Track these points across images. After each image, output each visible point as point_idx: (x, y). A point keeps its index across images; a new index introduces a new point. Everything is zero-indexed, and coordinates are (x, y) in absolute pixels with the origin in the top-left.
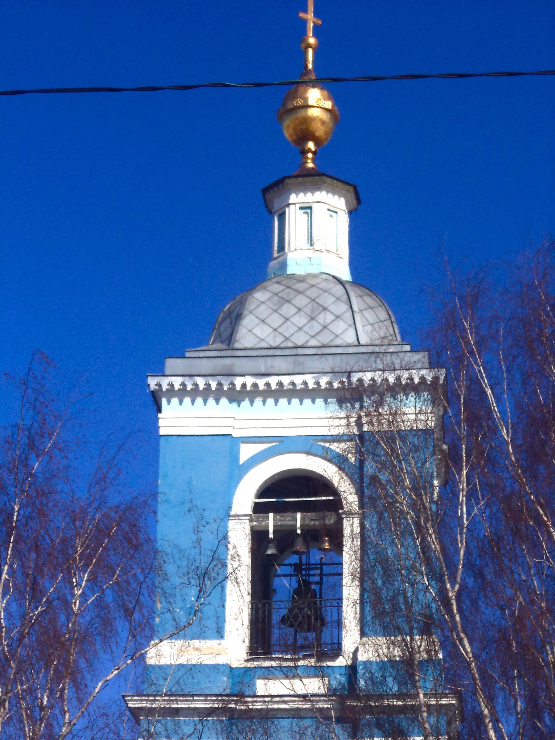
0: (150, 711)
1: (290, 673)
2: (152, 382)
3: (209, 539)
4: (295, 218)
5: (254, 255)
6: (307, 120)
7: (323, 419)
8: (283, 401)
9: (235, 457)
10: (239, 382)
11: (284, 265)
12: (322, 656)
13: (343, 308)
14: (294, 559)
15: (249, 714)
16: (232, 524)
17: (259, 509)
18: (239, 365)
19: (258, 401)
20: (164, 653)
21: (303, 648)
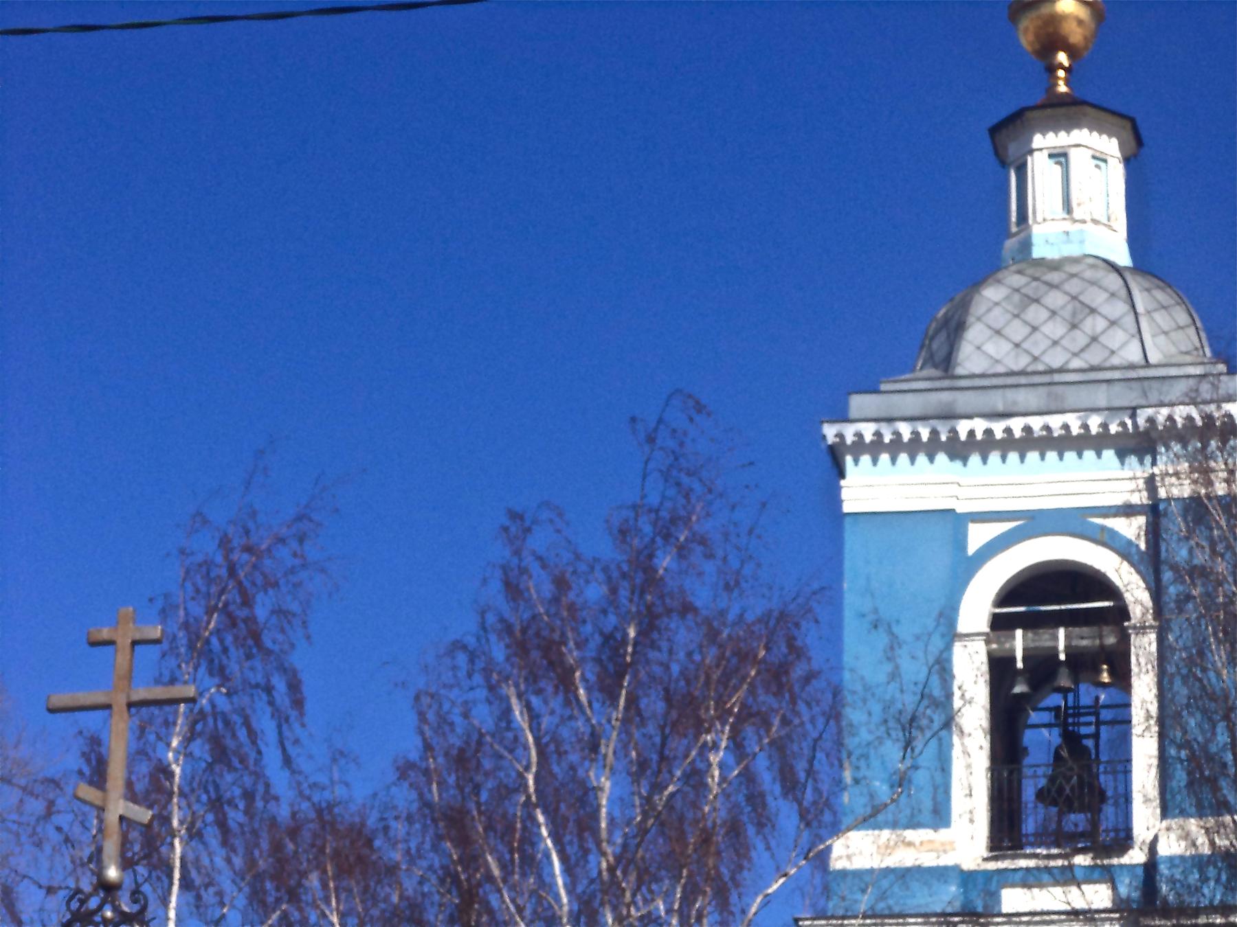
1: (1068, 877)
4: (1042, 171)
5: (987, 236)
7: (1109, 481)
8: (1033, 456)
9: (960, 541)
10: (963, 427)
11: (1027, 245)
13: (1119, 309)
14: (1055, 700)
17: (1000, 624)
18: (963, 401)
20: (856, 850)
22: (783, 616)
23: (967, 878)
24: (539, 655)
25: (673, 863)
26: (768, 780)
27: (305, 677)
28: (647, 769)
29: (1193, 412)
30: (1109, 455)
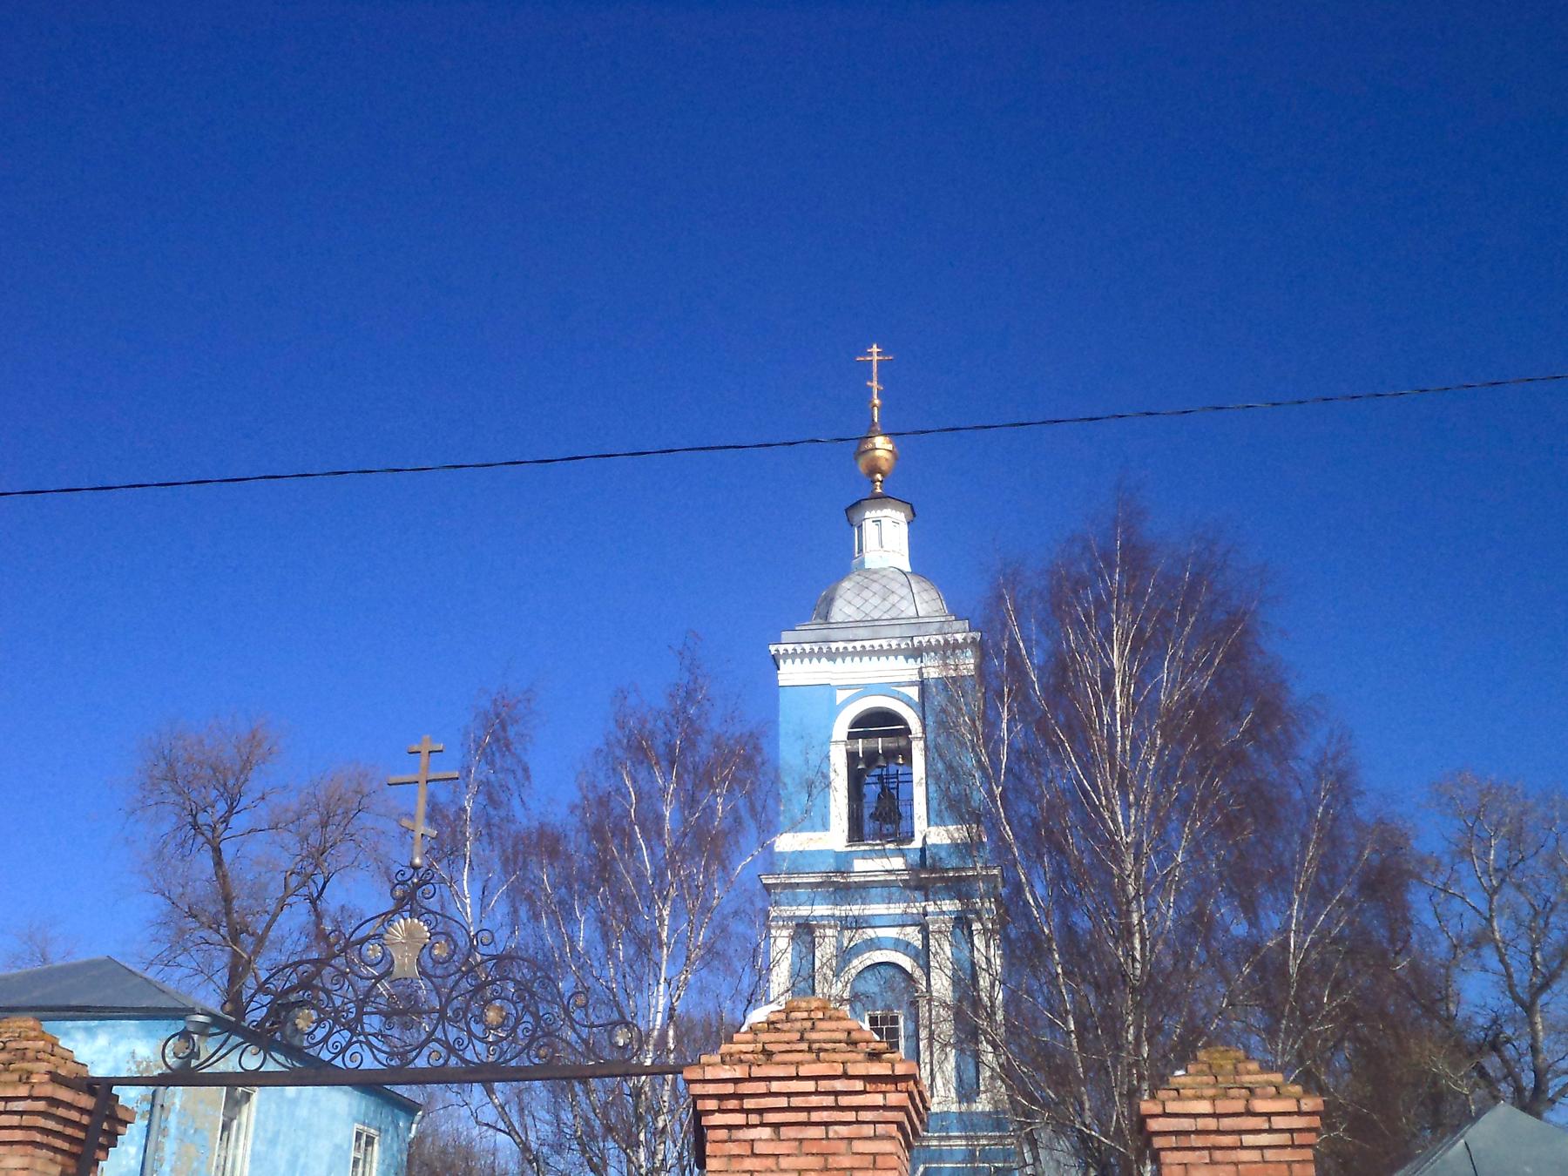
0: (775, 885)
1: (884, 854)
2: (773, 649)
3: (814, 758)
4: (869, 528)
5: (842, 558)
6: (876, 459)
7: (903, 670)
8: (866, 659)
9: (833, 698)
10: (834, 646)
11: (862, 562)
12: (901, 842)
13: (905, 591)
14: (878, 771)
15: (847, 887)
16: (832, 747)
17: (851, 736)
18: (834, 634)
19: (848, 659)
20: (786, 843)
21: (886, 836)
22: (751, 735)
23: (837, 855)
24: (639, 751)
25: (699, 849)
26: (744, 813)
27: (531, 766)
28: (691, 802)
29: (940, 638)
30: (901, 658)
